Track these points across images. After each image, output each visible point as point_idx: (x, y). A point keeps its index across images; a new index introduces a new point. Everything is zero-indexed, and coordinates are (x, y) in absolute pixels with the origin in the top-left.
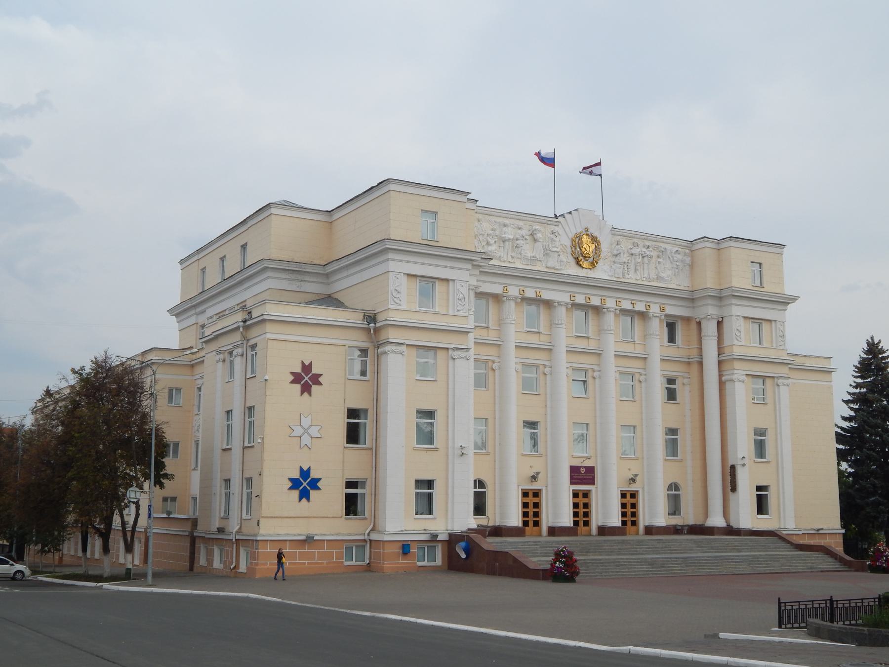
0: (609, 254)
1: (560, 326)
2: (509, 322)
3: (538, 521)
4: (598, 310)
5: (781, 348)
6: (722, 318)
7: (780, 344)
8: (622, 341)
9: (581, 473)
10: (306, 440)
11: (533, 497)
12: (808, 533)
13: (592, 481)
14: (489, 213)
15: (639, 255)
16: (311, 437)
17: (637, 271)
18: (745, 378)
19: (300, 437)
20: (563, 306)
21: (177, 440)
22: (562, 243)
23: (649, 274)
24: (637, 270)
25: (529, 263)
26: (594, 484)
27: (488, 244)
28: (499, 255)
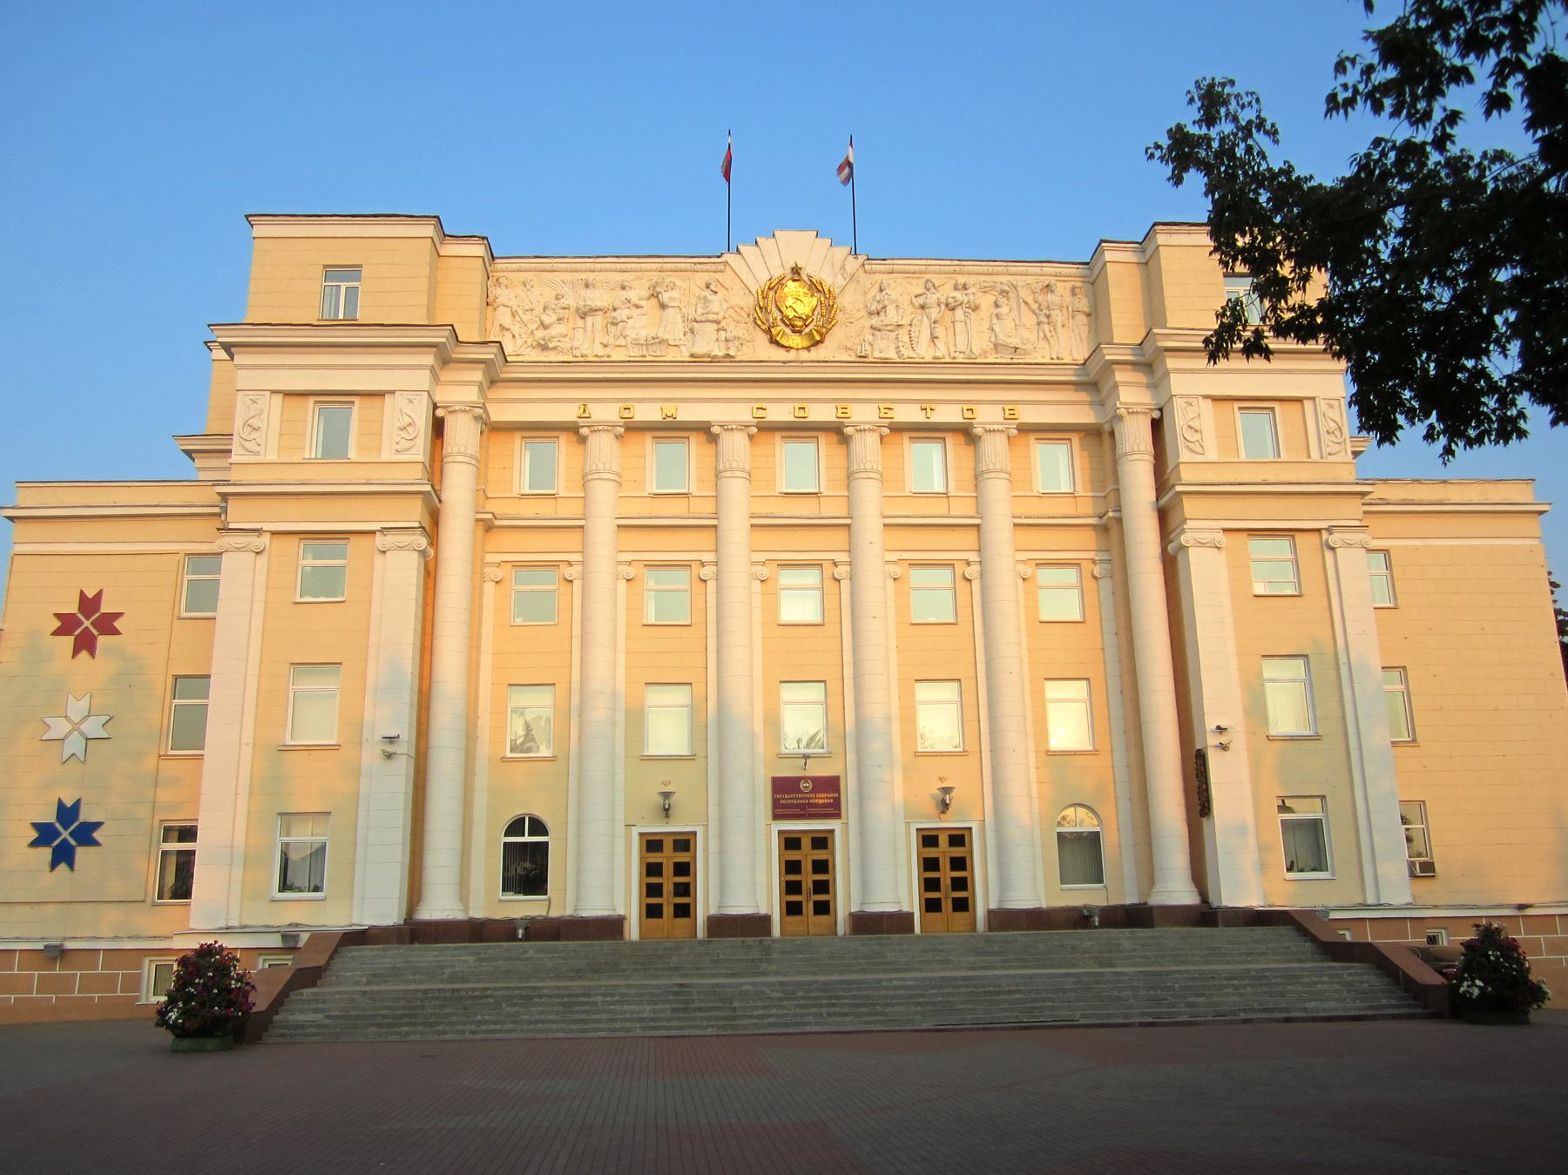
0: (863, 313)
2: (596, 476)
5: (1331, 459)
6: (1161, 410)
8: (911, 494)
9: (802, 792)
10: (75, 745)
12: (1411, 918)
13: (834, 810)
14: (548, 267)
15: (939, 305)
18: (1221, 538)
22: (732, 304)
24: (937, 338)
25: (645, 353)
26: (837, 815)
27: (544, 326)
28: (569, 345)
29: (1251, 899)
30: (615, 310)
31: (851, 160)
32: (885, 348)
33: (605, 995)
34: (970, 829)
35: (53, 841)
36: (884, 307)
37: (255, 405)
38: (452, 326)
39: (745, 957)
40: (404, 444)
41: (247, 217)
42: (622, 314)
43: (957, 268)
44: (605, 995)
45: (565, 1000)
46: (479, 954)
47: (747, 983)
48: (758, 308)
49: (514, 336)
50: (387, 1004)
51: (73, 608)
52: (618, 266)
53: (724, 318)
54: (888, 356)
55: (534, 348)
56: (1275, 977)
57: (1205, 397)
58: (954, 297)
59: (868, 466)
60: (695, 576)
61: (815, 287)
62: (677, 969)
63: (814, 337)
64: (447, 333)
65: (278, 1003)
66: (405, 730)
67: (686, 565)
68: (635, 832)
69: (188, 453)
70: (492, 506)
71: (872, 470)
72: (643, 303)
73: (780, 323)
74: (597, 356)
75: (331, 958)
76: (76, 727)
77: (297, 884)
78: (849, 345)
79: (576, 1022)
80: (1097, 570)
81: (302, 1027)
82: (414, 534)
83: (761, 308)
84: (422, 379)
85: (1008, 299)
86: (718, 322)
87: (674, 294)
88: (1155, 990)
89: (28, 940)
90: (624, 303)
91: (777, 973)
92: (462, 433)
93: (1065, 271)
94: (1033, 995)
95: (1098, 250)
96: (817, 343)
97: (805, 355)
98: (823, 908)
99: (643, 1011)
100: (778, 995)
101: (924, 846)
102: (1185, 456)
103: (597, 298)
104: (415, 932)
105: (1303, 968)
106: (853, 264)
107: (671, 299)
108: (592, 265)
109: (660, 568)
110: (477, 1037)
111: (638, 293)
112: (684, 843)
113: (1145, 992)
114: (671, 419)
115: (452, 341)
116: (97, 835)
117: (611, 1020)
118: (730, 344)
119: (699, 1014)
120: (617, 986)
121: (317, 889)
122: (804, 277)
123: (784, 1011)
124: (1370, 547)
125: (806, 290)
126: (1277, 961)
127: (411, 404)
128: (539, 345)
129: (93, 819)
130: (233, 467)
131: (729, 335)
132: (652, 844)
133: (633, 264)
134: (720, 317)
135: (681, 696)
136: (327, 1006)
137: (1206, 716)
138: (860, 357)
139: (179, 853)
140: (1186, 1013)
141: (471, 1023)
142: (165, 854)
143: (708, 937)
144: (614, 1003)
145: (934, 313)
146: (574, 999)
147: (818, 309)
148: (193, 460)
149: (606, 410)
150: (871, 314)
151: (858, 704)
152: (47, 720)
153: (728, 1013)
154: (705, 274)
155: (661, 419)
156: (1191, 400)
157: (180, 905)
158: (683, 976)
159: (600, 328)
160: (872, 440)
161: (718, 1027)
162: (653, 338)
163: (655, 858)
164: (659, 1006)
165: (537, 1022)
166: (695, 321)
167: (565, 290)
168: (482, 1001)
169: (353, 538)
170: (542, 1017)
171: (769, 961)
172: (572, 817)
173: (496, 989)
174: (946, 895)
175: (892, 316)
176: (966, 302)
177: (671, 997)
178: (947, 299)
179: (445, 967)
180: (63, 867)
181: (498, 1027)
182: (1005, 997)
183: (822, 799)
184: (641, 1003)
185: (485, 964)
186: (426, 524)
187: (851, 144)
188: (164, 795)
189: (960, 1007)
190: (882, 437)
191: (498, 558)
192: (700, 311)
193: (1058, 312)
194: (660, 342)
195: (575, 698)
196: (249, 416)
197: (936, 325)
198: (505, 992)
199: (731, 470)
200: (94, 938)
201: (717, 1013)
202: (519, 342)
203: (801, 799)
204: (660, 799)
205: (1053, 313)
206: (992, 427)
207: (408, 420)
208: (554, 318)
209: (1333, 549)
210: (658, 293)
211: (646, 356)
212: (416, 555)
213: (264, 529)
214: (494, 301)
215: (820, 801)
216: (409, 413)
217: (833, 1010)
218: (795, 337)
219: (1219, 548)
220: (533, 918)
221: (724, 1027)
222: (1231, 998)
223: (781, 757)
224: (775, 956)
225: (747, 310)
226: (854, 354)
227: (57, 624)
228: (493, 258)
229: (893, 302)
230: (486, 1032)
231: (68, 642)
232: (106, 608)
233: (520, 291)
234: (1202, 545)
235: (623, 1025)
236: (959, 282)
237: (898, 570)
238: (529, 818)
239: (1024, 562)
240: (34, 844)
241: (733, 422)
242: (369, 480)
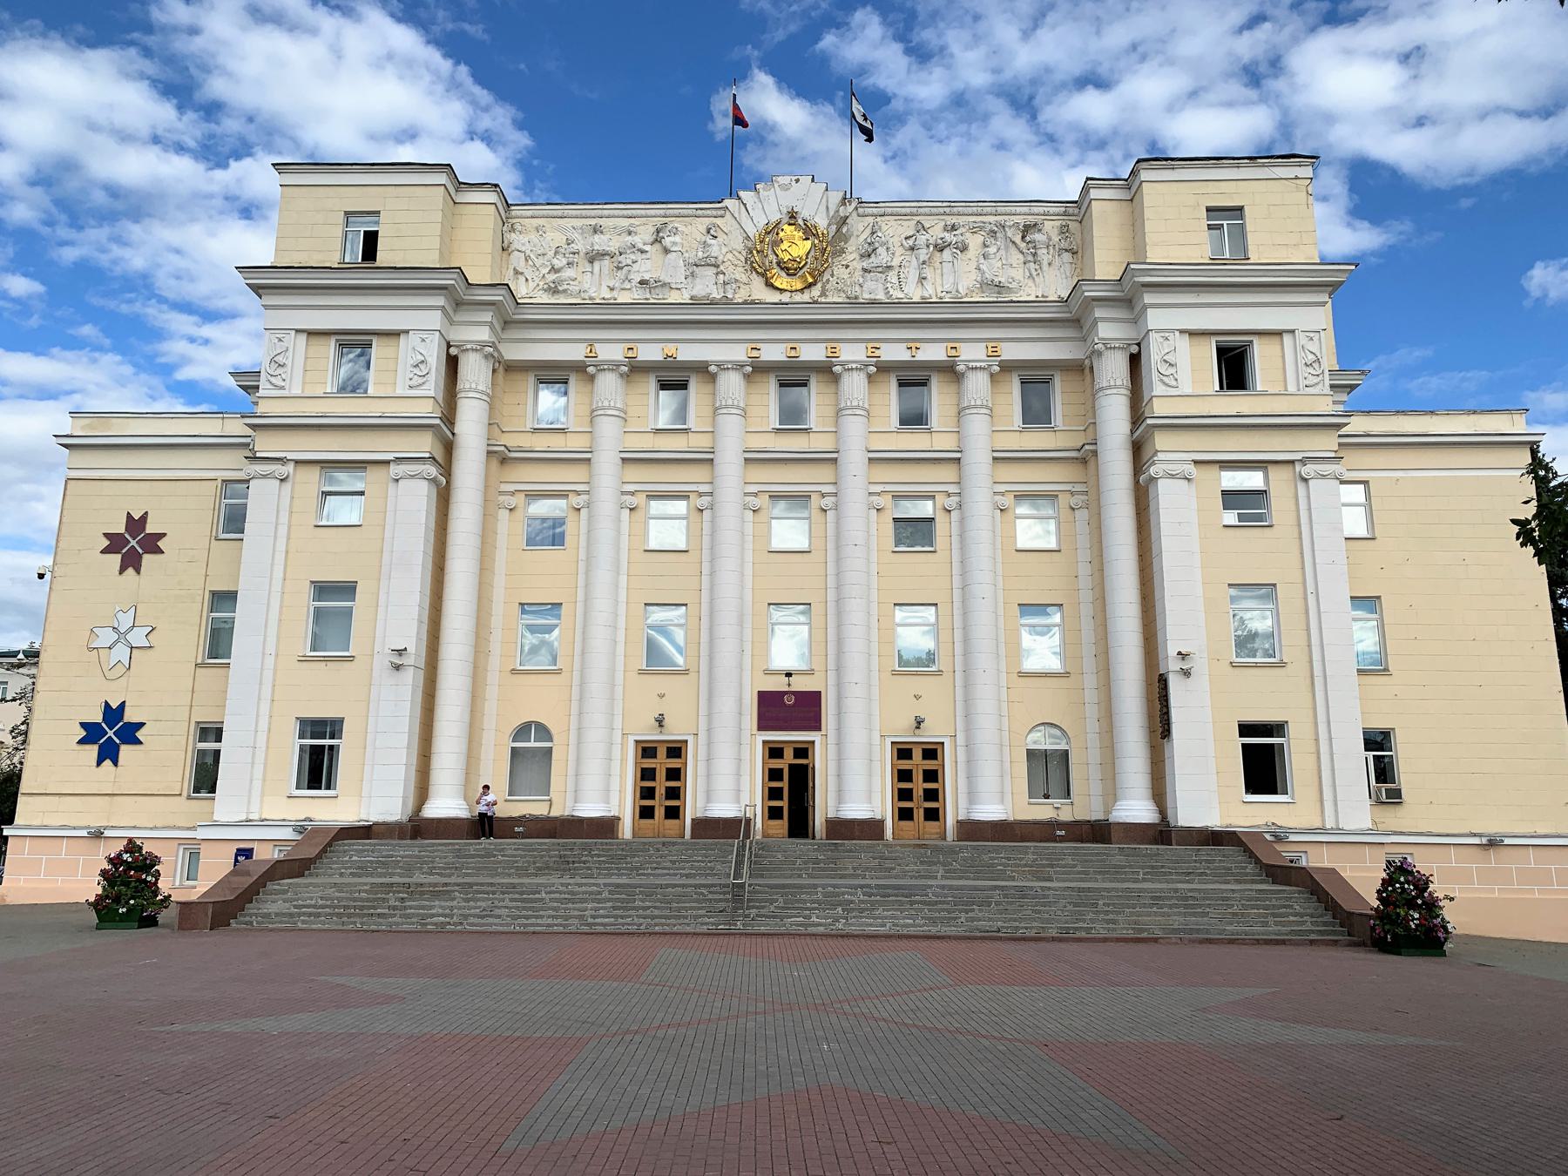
1: (725, 411)
3: (679, 807)
6: (1139, 345)
7: (1307, 383)
11: (668, 757)
13: (815, 724)
14: (560, 213)
15: (928, 246)
18: (1191, 469)
19: (132, 648)
23: (956, 284)
25: (648, 296)
27: (554, 270)
28: (577, 288)
29: (1213, 819)
32: (874, 289)
37: (282, 343)
38: (460, 268)
43: (947, 210)
49: (527, 280)
52: (625, 212)
54: (877, 297)
57: (1182, 332)
60: (692, 506)
61: (809, 232)
63: (806, 280)
71: (858, 407)
72: (647, 248)
73: (775, 266)
74: (604, 299)
80: (1073, 501)
82: (424, 464)
84: (434, 320)
85: (996, 239)
87: (677, 239)
90: (629, 248)
92: (474, 372)
93: (1052, 210)
95: (1085, 190)
97: (798, 297)
98: (933, 815)
101: (899, 758)
102: (1159, 389)
103: (600, 242)
107: (674, 243)
108: (600, 211)
111: (644, 235)
114: (672, 359)
115: (463, 284)
116: (139, 735)
122: (800, 222)
124: (1345, 478)
125: (801, 234)
127: (423, 343)
128: (550, 287)
130: (260, 401)
143: (692, 838)
145: (923, 254)
147: (812, 253)
149: (612, 352)
155: (662, 359)
156: (1167, 335)
159: (607, 272)
163: (649, 763)
167: (576, 235)
175: (882, 257)
193: (1045, 251)
194: (662, 286)
196: (275, 353)
205: (1039, 252)
206: (974, 364)
208: (565, 261)
209: (1305, 480)
211: (649, 299)
213: (288, 458)
214: (509, 247)
216: (422, 351)
219: (1189, 480)
223: (769, 672)
232: (151, 528)
233: (533, 236)
234: (1173, 476)
239: (1002, 494)
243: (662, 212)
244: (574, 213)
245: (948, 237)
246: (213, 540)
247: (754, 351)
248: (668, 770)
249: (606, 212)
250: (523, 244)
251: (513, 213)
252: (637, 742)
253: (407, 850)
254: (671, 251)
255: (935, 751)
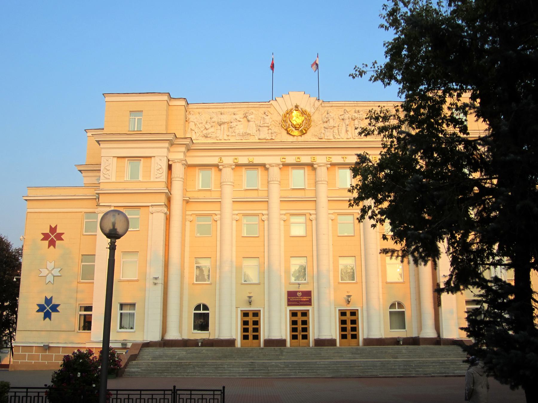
0: (321, 122)
2: (225, 183)
4: (311, 166)
9: (298, 296)
10: (50, 278)
14: (208, 107)
16: (54, 276)
17: (348, 132)
20: (274, 167)
21: (338, 314)
24: (348, 131)
25: (242, 139)
26: (310, 305)
28: (215, 136)
30: (231, 123)
31: (317, 62)
32: (329, 135)
33: (228, 365)
34: (358, 310)
35: (44, 311)
36: (329, 120)
38: (175, 133)
39: (275, 354)
40: (159, 175)
41: (103, 94)
42: (234, 124)
43: (356, 105)
44: (228, 365)
45: (215, 366)
46: (187, 351)
47: (274, 362)
48: (283, 121)
49: (195, 133)
50: (159, 366)
51: (48, 231)
53: (271, 125)
55: (203, 137)
56: (448, 363)
58: (354, 116)
59: (322, 179)
61: (303, 113)
62: (251, 357)
64: (173, 136)
65: (126, 365)
66: (160, 274)
67: (257, 215)
68: (239, 310)
69: (80, 171)
70: (189, 195)
71: (324, 181)
72: (241, 120)
73: (291, 126)
75: (139, 351)
76: (50, 272)
77: (125, 326)
78: (316, 134)
79: (219, 373)
81: (134, 373)
83: (284, 121)
86: (268, 127)
87: (252, 116)
88: (407, 366)
89: (38, 343)
91: (285, 359)
92: (178, 169)
94: (366, 368)
96: (304, 134)
98: (305, 337)
99: (240, 370)
100: (283, 366)
103: (225, 118)
104: (165, 343)
105: (458, 360)
106: (317, 104)
109: (248, 216)
110: (188, 377)
112: (256, 314)
113: (403, 367)
114: (251, 163)
115: (175, 138)
117: (230, 373)
118: (273, 135)
119: (257, 372)
120: (232, 362)
121: (132, 328)
122: (300, 109)
123: (284, 371)
125: (300, 114)
126: (455, 357)
128: (205, 136)
129: (57, 303)
131: (272, 131)
132: (245, 314)
133: (237, 105)
134: (269, 125)
135: (254, 262)
136: (141, 366)
137: (440, 271)
138: (320, 139)
139: (85, 315)
140: (414, 374)
141: (186, 373)
142: (80, 315)
144: (230, 368)
145: (347, 122)
146: (218, 366)
147: (305, 121)
148: (82, 173)
149: (228, 160)
150: (324, 122)
151: (318, 266)
152: (40, 269)
153: (267, 371)
154: (264, 109)
155: (248, 163)
157: (88, 333)
158: (254, 360)
160: (324, 169)
161: (263, 376)
162: (245, 133)
163: (246, 319)
164: (245, 369)
165: (206, 373)
166: (260, 126)
168: (189, 366)
169: (141, 208)
170: (208, 371)
171: (282, 355)
172: (217, 305)
173: (193, 362)
174: (349, 333)
175: (331, 123)
176: (359, 117)
177: (249, 366)
178: (352, 116)
179: (177, 355)
180: (47, 319)
181: (194, 374)
182: (356, 368)
183: (305, 299)
184: (239, 368)
185: (189, 355)
186: (166, 204)
187: (318, 57)
188: (80, 296)
189: (341, 371)
190: (328, 168)
191: (191, 213)
192: (262, 122)
194: (247, 135)
195: (218, 263)
196: (106, 166)
197: (348, 126)
198: (196, 363)
199: (273, 181)
200: (58, 343)
201: (263, 371)
202: (198, 135)
203: (297, 299)
204: (248, 299)
207: (160, 167)
210: (247, 116)
212: (163, 214)
214: (188, 120)
215: (304, 300)
217: (300, 371)
218: (296, 132)
220: (204, 339)
221: (265, 375)
222: (431, 369)
223: (291, 284)
224: (284, 353)
225: (279, 122)
226: (317, 138)
227: (42, 237)
228: (188, 104)
229: (332, 118)
230: (191, 375)
231: (46, 243)
232: (58, 231)
235: (233, 374)
236: (356, 110)
237: (333, 217)
238: (203, 305)
240: (38, 311)
241: (274, 164)
242: (147, 188)
243: (247, 106)
244: (213, 106)
245: (356, 115)
246: (82, 235)
247: (284, 159)
248: (253, 321)
249: (225, 106)
250: (194, 119)
251: (190, 107)
252: (241, 311)
253: (158, 351)
254: (250, 121)
255: (355, 312)
